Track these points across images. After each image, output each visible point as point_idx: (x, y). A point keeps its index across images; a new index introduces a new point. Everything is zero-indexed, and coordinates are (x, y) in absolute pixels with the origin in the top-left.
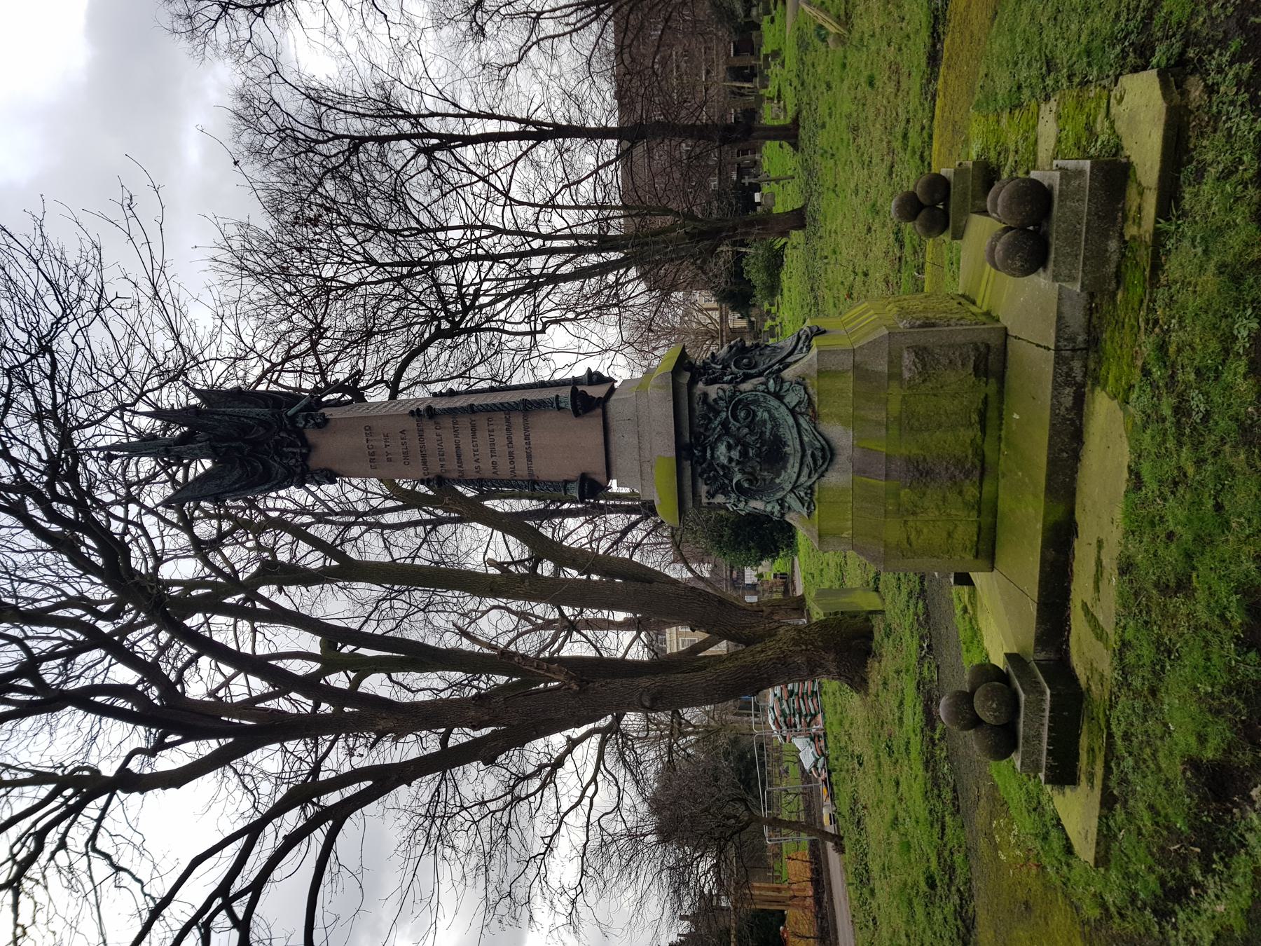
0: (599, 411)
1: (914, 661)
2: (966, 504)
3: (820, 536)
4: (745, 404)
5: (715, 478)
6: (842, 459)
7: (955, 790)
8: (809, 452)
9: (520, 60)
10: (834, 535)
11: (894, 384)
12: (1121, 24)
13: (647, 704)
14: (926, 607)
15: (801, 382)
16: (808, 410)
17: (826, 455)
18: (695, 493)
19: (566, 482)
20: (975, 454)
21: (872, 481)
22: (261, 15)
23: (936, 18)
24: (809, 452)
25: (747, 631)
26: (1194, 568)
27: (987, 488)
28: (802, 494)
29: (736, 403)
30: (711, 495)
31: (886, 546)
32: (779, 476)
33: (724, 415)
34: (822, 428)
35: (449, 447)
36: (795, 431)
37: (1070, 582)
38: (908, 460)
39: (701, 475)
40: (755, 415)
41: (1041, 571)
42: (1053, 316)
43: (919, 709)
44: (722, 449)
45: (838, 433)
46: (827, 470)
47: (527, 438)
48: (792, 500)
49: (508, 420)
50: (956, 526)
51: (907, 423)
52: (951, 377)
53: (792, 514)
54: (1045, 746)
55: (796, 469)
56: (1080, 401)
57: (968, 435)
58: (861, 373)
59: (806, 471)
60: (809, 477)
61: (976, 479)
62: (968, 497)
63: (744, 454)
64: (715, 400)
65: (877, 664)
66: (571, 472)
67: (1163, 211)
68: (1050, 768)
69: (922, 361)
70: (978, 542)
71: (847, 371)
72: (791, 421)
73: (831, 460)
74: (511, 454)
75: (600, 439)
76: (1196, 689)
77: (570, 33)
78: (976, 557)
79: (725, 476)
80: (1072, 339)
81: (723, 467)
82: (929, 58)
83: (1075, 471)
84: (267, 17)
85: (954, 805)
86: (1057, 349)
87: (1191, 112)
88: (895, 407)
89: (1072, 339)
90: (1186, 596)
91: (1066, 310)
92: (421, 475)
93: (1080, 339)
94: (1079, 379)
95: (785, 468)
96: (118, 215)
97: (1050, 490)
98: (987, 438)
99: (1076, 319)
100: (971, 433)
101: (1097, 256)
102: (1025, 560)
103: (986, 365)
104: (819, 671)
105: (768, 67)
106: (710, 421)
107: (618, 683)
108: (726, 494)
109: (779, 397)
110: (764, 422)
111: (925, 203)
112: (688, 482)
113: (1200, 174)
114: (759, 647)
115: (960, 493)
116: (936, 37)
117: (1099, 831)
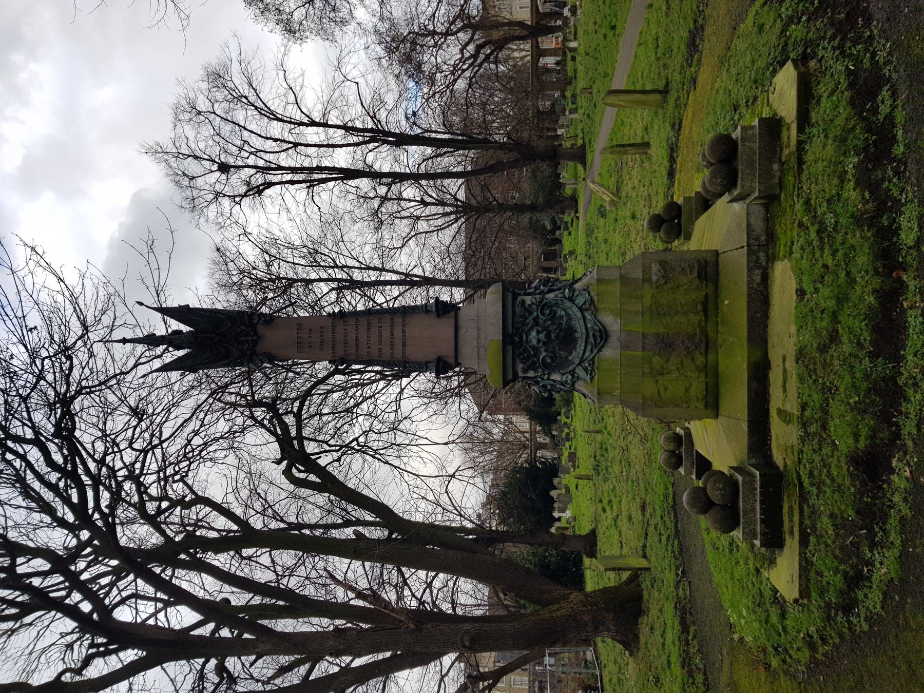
0: (453, 314)
1: (672, 589)
2: (697, 367)
3: (598, 394)
4: (548, 305)
5: (528, 357)
6: (614, 339)
7: (705, 674)
8: (591, 333)
9: (403, 246)
11: (647, 285)
12: (772, 55)
13: (467, 644)
14: (680, 544)
15: (586, 289)
16: (591, 306)
19: (427, 362)
20: (701, 332)
21: (634, 353)
22: (239, 203)
23: (672, 149)
24: (591, 333)
25: (546, 596)
26: (839, 322)
27: (711, 357)
28: (587, 365)
29: (543, 306)
30: (525, 371)
31: (644, 398)
32: (571, 353)
33: (535, 314)
34: (600, 317)
35: (351, 338)
36: (582, 322)
37: (768, 404)
38: (657, 335)
39: (519, 356)
40: (556, 313)
42: (744, 225)
43: (677, 623)
44: (534, 333)
45: (611, 321)
46: (603, 347)
47: (404, 332)
48: (580, 372)
49: (392, 320)
50: (691, 384)
51: (656, 312)
52: (684, 280)
53: (580, 382)
54: (758, 516)
55: (583, 348)
56: (766, 279)
57: (695, 319)
58: (625, 280)
59: (589, 347)
60: (592, 351)
61: (703, 350)
62: (698, 363)
63: (548, 336)
64: (529, 305)
65: (646, 618)
66: (432, 356)
67: (801, 130)
68: (763, 534)
69: (664, 268)
70: (706, 395)
71: (616, 280)
72: (579, 315)
73: (606, 340)
74: (392, 343)
75: (452, 333)
76: (849, 403)
77: (438, 230)
78: (706, 406)
79: (535, 355)
80: (757, 238)
81: (534, 348)
82: (669, 175)
84: (242, 203)
85: (704, 685)
86: (749, 245)
87: (811, 74)
88: (647, 301)
89: (757, 238)
90: (837, 345)
91: (752, 220)
93: (763, 238)
94: (764, 264)
95: (575, 348)
96: (145, 250)
97: (750, 339)
98: (709, 323)
101: (766, 175)
102: (737, 398)
103: (706, 273)
105: (566, 262)
106: (526, 318)
107: (445, 626)
108: (535, 370)
109: (571, 299)
110: (562, 317)
111: (666, 218)
113: (819, 101)
114: (555, 607)
115: (693, 359)
116: (672, 160)
117: (800, 565)
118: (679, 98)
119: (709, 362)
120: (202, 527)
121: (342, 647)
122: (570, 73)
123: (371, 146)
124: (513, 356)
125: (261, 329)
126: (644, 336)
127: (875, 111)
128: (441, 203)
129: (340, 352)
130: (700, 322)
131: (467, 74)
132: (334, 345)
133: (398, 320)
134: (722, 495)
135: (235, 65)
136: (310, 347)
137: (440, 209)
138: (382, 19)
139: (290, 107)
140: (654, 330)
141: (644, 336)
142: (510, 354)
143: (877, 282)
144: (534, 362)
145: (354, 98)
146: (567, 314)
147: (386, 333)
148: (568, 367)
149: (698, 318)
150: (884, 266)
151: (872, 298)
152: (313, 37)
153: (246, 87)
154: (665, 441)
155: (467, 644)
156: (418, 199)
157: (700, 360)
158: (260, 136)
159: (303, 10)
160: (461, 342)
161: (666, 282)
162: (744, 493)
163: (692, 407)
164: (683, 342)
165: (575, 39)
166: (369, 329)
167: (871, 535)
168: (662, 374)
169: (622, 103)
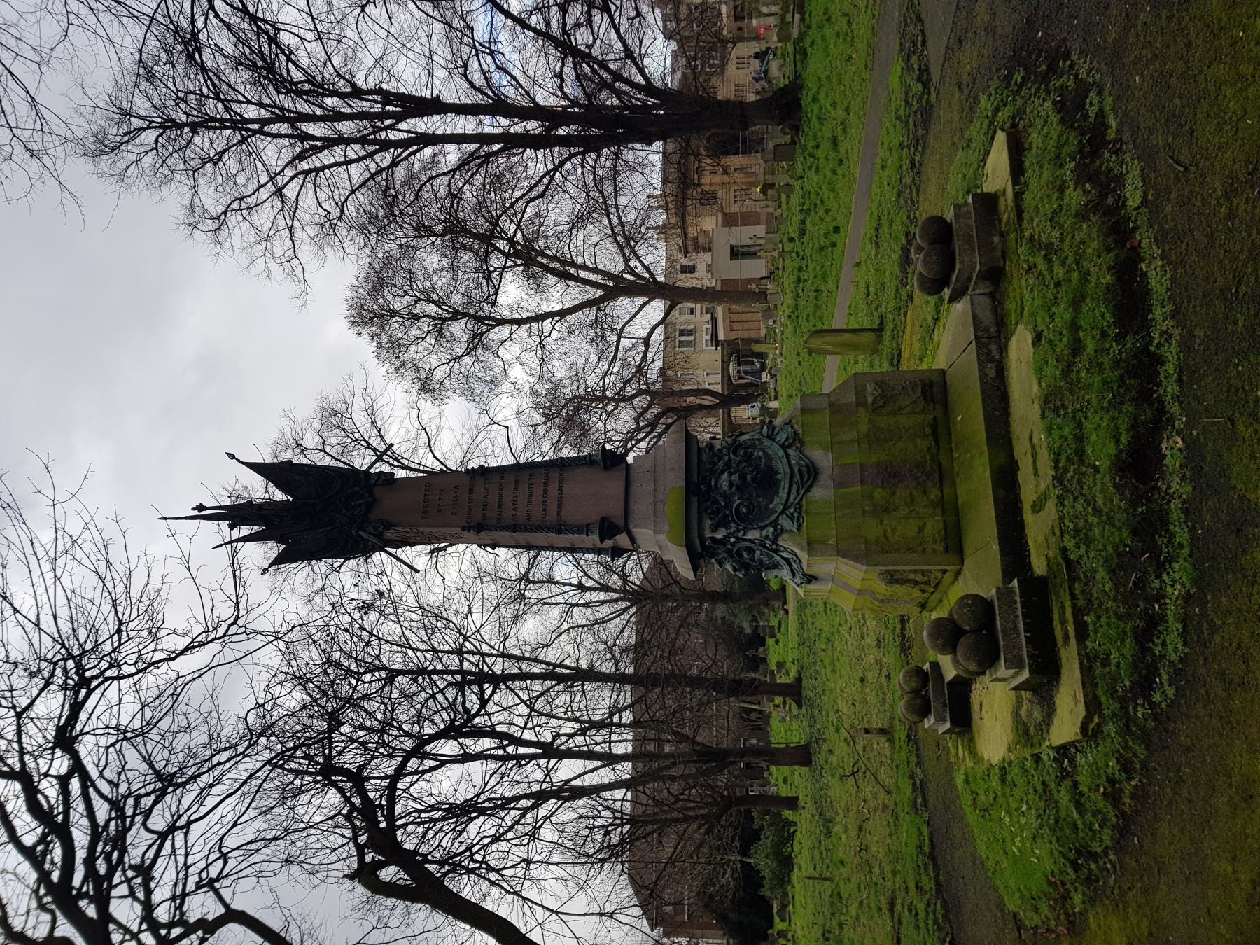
3: (809, 543)
5: (718, 511)
6: (824, 477)
8: (796, 470)
10: (821, 542)
15: (789, 423)
16: (796, 441)
17: (810, 474)
18: (700, 523)
24: (796, 470)
31: (866, 542)
33: (726, 458)
34: (806, 452)
39: (706, 510)
40: (752, 454)
41: (998, 529)
42: (970, 319)
45: (820, 456)
46: (811, 486)
47: (560, 489)
48: (785, 522)
49: (547, 475)
53: (785, 536)
57: (923, 444)
59: (795, 487)
62: (932, 496)
72: (781, 453)
73: (815, 478)
74: (544, 502)
75: (622, 489)
78: (947, 550)
83: (1008, 424)
86: (977, 338)
88: (864, 427)
89: (986, 330)
92: (464, 523)
94: (997, 357)
95: (777, 493)
99: (987, 318)
106: (715, 464)
108: (726, 526)
109: (771, 437)
112: (694, 515)
115: (925, 492)
118: (895, 326)
119: (946, 498)
124: (699, 513)
125: (378, 492)
126: (862, 467)
127: (1086, 116)
128: (604, 588)
129: (477, 516)
130: (929, 449)
131: (643, 445)
132: (470, 508)
133: (555, 475)
134: (973, 612)
135: (358, 399)
136: (439, 511)
137: (602, 596)
138: (541, 378)
139: (422, 451)
140: (874, 460)
141: (862, 467)
144: (726, 516)
145: (502, 441)
146: (766, 454)
147: (538, 491)
148: (768, 517)
149: (927, 443)
150: (1116, 241)
151: (1109, 277)
152: (456, 397)
153: (369, 425)
154: (904, 676)
156: (575, 582)
157: (934, 493)
159: (446, 368)
160: (632, 499)
161: (884, 406)
162: (1000, 607)
163: (930, 550)
164: (911, 471)
165: (776, 398)
166: (516, 487)
167: (1155, 551)
168: (887, 510)
169: (829, 348)
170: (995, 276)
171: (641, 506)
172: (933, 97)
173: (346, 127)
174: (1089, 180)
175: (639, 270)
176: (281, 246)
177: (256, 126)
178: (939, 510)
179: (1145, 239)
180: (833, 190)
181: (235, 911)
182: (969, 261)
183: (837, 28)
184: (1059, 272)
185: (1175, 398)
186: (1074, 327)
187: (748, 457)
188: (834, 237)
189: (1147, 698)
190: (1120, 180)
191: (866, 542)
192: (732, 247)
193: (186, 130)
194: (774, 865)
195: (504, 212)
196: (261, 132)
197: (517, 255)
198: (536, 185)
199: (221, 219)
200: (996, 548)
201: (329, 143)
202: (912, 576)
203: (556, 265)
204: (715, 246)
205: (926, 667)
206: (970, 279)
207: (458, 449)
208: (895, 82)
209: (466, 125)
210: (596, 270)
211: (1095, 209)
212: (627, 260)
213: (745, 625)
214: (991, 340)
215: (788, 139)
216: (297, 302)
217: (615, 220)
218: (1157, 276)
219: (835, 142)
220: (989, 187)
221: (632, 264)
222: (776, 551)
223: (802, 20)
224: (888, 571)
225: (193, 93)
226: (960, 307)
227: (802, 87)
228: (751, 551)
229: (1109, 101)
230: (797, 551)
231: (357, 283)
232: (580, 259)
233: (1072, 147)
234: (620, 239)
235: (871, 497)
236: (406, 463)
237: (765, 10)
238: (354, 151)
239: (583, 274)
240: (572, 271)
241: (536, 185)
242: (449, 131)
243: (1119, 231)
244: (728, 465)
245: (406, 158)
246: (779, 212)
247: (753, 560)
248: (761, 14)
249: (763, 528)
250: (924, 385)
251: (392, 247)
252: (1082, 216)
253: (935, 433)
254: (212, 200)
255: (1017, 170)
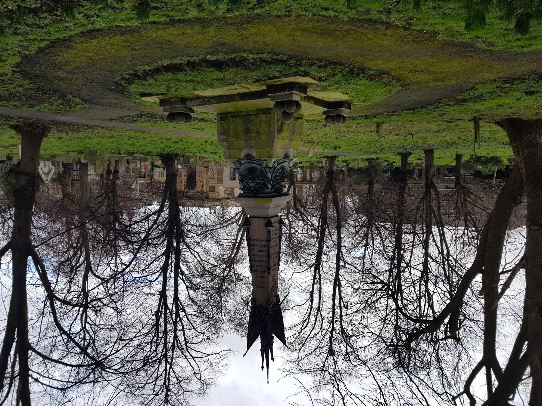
5: (262, 187)
6: (249, 152)
17: (249, 156)
20: (242, 117)
27: (252, 113)
31: (268, 139)
45: (243, 153)
47: (256, 240)
48: (264, 165)
49: (252, 245)
66: (265, 229)
72: (243, 166)
78: (270, 113)
80: (201, 102)
86: (203, 105)
88: (234, 139)
89: (201, 102)
91: (196, 104)
92: (267, 274)
99: (197, 102)
100: (238, 119)
104: (534, 142)
112: (263, 195)
120: (65, 261)
121: (537, 309)
122: (308, 165)
123: (321, 269)
125: (257, 304)
127: (130, 78)
133: (252, 242)
140: (243, 136)
142: (261, 195)
143: (165, 73)
155: (537, 228)
156: (364, 248)
158: (313, 328)
160: (260, 216)
166: (256, 255)
168: (258, 132)
170: (183, 100)
171: (261, 213)
172: (146, 113)
173: (170, 327)
174: (146, 78)
175: (237, 217)
176: (214, 359)
177: (168, 366)
178: (258, 116)
179: (159, 64)
180: (193, 143)
181: (465, 389)
182: (179, 108)
183: (135, 142)
184: (173, 85)
185: (197, 57)
186: (187, 81)
187: (245, 177)
188: (209, 142)
189: (286, 61)
190: (144, 70)
191: (268, 139)
192: (231, 179)
193: (169, 393)
194: (490, 164)
195: (346, 315)
196: (171, 364)
197: (230, 267)
198: (194, 256)
199: (205, 384)
200: (263, 99)
201: (176, 337)
202: (280, 124)
203: (235, 250)
204: (232, 187)
205: (325, 116)
206: (185, 107)
207: (301, 293)
208: (144, 125)
209: (171, 282)
210: (237, 235)
211: (153, 77)
212: (233, 222)
213: (386, 175)
214: (204, 101)
215: (182, 159)
216: (236, 354)
217: (217, 227)
218: (165, 63)
219: (175, 142)
220: (158, 101)
221: (234, 220)
222: (275, 168)
223: (136, 153)
224: (278, 132)
225: (154, 388)
226: (195, 109)
227: (161, 153)
228: (276, 176)
229: (124, 73)
230: (273, 161)
231: (240, 335)
232: (233, 241)
233: (139, 81)
234: (225, 224)
235: (254, 137)
236: (307, 316)
237: (139, 166)
238: (179, 327)
239: (238, 240)
240: (237, 245)
241: (194, 256)
242: (173, 289)
243: (158, 71)
244: (247, 183)
245: (182, 306)
246: (212, 162)
247: (279, 176)
248: (140, 168)
249: (266, 172)
250: (221, 120)
251: (226, 319)
252: (156, 80)
253: (235, 117)
254: (195, 385)
255: (150, 95)
